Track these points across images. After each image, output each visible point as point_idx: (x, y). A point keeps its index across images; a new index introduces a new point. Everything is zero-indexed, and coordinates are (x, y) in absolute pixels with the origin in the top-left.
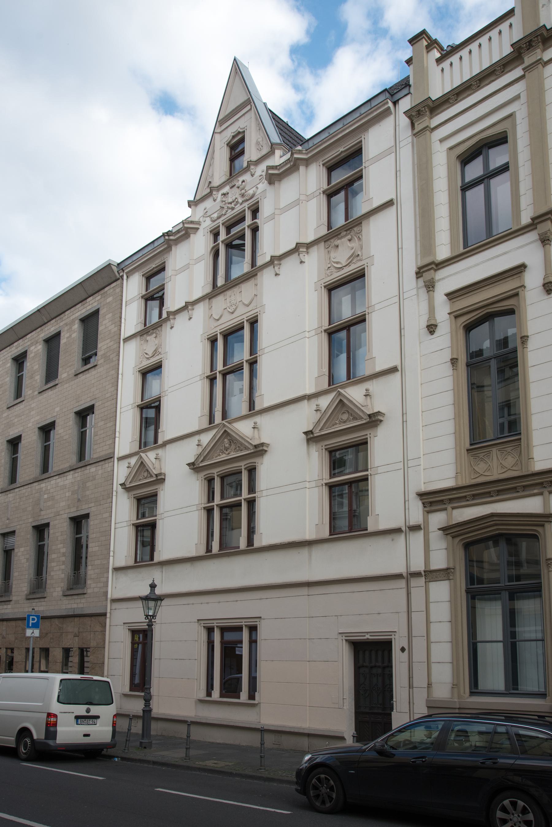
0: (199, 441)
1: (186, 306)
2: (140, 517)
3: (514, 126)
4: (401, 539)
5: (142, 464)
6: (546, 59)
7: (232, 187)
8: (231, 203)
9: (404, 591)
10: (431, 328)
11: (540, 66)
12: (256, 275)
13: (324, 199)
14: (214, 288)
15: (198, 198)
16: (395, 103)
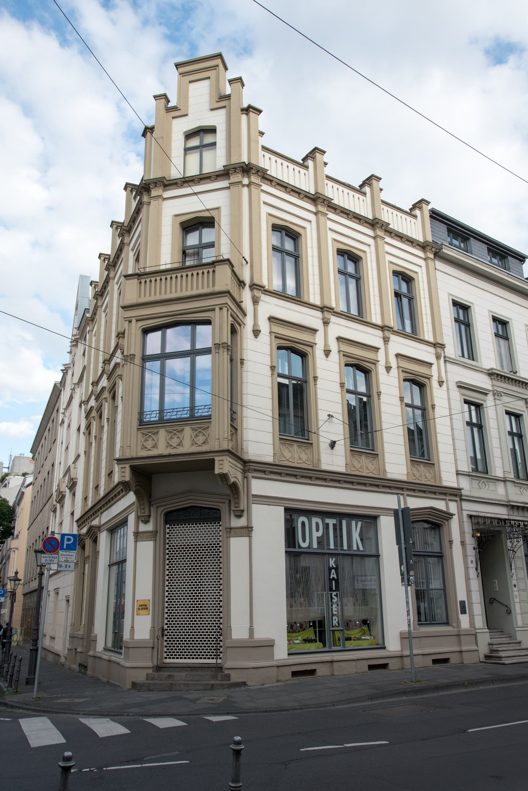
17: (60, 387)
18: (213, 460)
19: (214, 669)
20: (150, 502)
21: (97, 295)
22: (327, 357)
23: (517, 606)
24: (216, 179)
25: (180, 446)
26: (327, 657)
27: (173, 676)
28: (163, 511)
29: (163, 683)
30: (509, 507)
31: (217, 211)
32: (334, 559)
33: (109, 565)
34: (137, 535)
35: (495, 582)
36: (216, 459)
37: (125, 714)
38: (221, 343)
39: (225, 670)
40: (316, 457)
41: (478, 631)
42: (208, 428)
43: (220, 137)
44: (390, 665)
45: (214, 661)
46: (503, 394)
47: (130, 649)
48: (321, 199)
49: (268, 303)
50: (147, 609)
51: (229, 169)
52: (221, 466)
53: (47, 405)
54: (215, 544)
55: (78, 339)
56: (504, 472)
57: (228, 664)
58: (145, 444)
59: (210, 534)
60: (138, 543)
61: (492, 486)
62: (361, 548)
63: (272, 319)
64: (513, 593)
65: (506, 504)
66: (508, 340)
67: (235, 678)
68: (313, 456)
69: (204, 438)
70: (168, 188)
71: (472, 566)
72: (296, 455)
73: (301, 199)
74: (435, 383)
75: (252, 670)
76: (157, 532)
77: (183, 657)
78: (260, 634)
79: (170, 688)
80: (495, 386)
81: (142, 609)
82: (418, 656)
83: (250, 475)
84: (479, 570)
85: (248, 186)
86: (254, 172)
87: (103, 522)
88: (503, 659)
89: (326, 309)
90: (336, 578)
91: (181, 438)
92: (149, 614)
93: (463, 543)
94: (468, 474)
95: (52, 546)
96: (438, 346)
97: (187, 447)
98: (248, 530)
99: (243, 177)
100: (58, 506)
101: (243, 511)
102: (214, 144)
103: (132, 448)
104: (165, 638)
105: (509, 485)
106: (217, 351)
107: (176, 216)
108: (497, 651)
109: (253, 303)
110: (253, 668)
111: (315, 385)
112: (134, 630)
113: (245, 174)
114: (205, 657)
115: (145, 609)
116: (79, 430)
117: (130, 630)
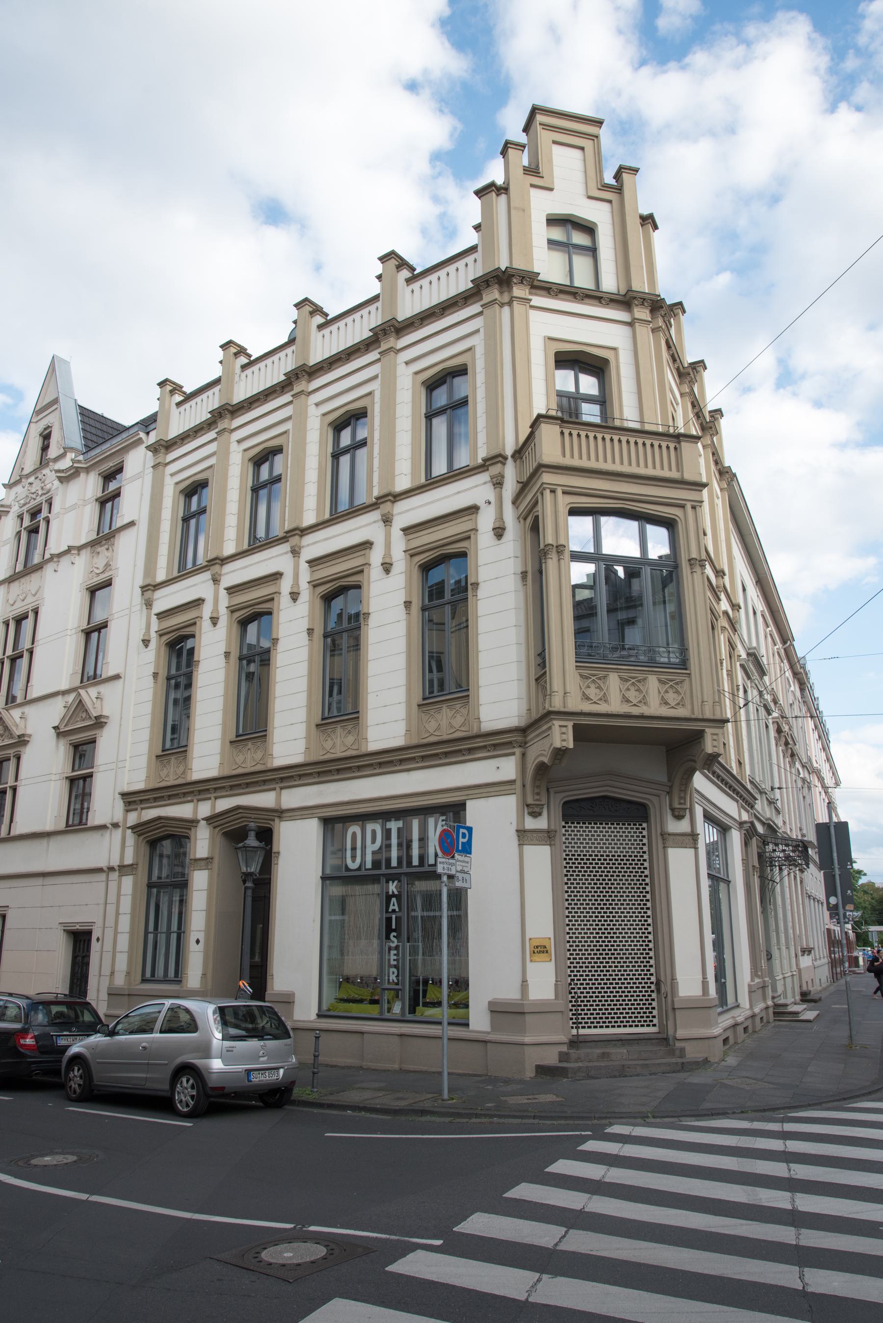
0: (23, 713)
1: (69, 549)
2: (76, 767)
3: (373, 403)
4: (107, 834)
5: (80, 704)
6: (399, 346)
7: (36, 478)
8: (33, 493)
9: (103, 885)
10: (146, 642)
11: (392, 353)
12: (42, 567)
13: (97, 507)
14: (24, 567)
15: (12, 481)
16: (148, 433)
19: (657, 1041)
28: (562, 799)
32: (396, 882)
47: (526, 1015)
51: (635, 298)
57: (681, 1033)
77: (634, 1024)
81: (540, 952)
90: (397, 910)
91: (644, 692)
115: (543, 952)
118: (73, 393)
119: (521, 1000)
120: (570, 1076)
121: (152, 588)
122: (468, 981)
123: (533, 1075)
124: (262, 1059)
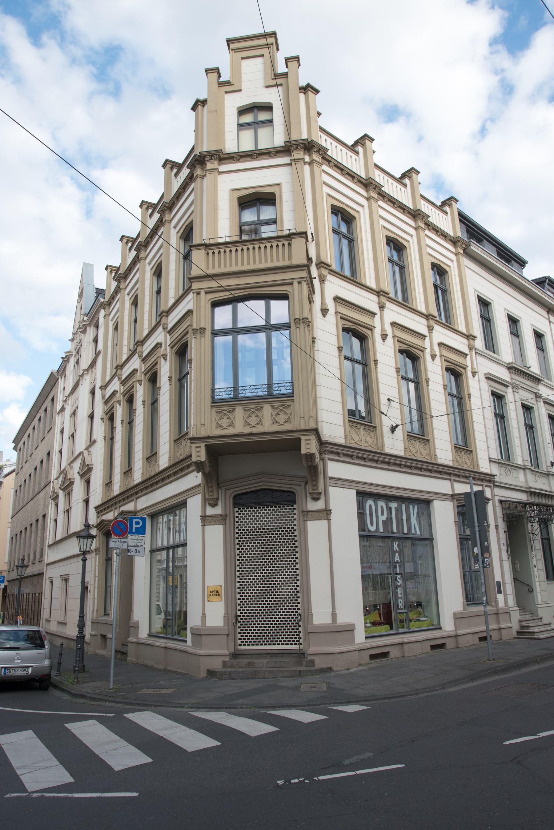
17: (57, 376)
18: (299, 439)
19: (297, 655)
20: (218, 484)
21: (120, 277)
22: (384, 341)
23: (537, 584)
24: (275, 155)
25: (260, 425)
26: (397, 639)
27: (253, 663)
29: (245, 671)
30: (529, 493)
31: (278, 187)
33: (150, 551)
34: (205, 519)
35: (517, 563)
36: (303, 438)
37: (238, 707)
38: (301, 318)
39: (308, 656)
40: (380, 440)
41: (511, 609)
42: (290, 406)
43: (278, 114)
44: (447, 644)
45: (297, 647)
46: (520, 387)
47: (202, 636)
48: (373, 185)
49: (333, 283)
50: (219, 595)
52: (308, 446)
53: (39, 395)
54: (256, 529)
55: (86, 326)
56: (523, 460)
58: (220, 423)
59: (280, 518)
60: (206, 527)
61: (514, 473)
62: (418, 532)
63: (337, 299)
64: (534, 573)
65: (526, 490)
66: (519, 337)
67: (320, 663)
68: (377, 439)
69: (286, 417)
70: (223, 162)
71: (504, 548)
72: (363, 438)
73: (355, 183)
74: (470, 374)
75: (337, 655)
76: (227, 515)
78: (342, 619)
79: (255, 676)
80: (514, 379)
81: (214, 595)
82: (469, 635)
83: (327, 456)
84: (509, 553)
85: (310, 164)
86: (315, 150)
87: (139, 507)
88: (536, 634)
89: (382, 293)
91: (261, 418)
92: (221, 600)
93: (497, 527)
94: (497, 461)
95: (121, 529)
96: (470, 337)
97: (268, 426)
98: (326, 513)
99: (305, 154)
100: (61, 494)
101: (320, 493)
102: (271, 121)
103: (206, 425)
104: (239, 624)
105: (528, 472)
106: (298, 326)
107: (233, 190)
108: (528, 627)
109: (320, 282)
110: (339, 653)
111: (376, 368)
112: (205, 617)
113: (306, 151)
114: (249, 643)
115: (217, 595)
116: (91, 417)
117: (224, 616)
118: (93, 282)
119: (202, 626)
120: (218, 677)
121: (104, 388)
122: (186, 613)
123: (205, 675)
124: (16, 661)
